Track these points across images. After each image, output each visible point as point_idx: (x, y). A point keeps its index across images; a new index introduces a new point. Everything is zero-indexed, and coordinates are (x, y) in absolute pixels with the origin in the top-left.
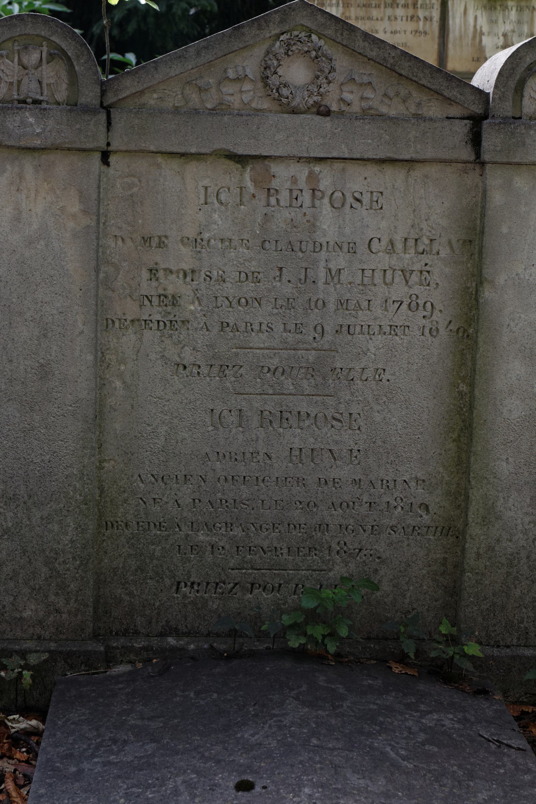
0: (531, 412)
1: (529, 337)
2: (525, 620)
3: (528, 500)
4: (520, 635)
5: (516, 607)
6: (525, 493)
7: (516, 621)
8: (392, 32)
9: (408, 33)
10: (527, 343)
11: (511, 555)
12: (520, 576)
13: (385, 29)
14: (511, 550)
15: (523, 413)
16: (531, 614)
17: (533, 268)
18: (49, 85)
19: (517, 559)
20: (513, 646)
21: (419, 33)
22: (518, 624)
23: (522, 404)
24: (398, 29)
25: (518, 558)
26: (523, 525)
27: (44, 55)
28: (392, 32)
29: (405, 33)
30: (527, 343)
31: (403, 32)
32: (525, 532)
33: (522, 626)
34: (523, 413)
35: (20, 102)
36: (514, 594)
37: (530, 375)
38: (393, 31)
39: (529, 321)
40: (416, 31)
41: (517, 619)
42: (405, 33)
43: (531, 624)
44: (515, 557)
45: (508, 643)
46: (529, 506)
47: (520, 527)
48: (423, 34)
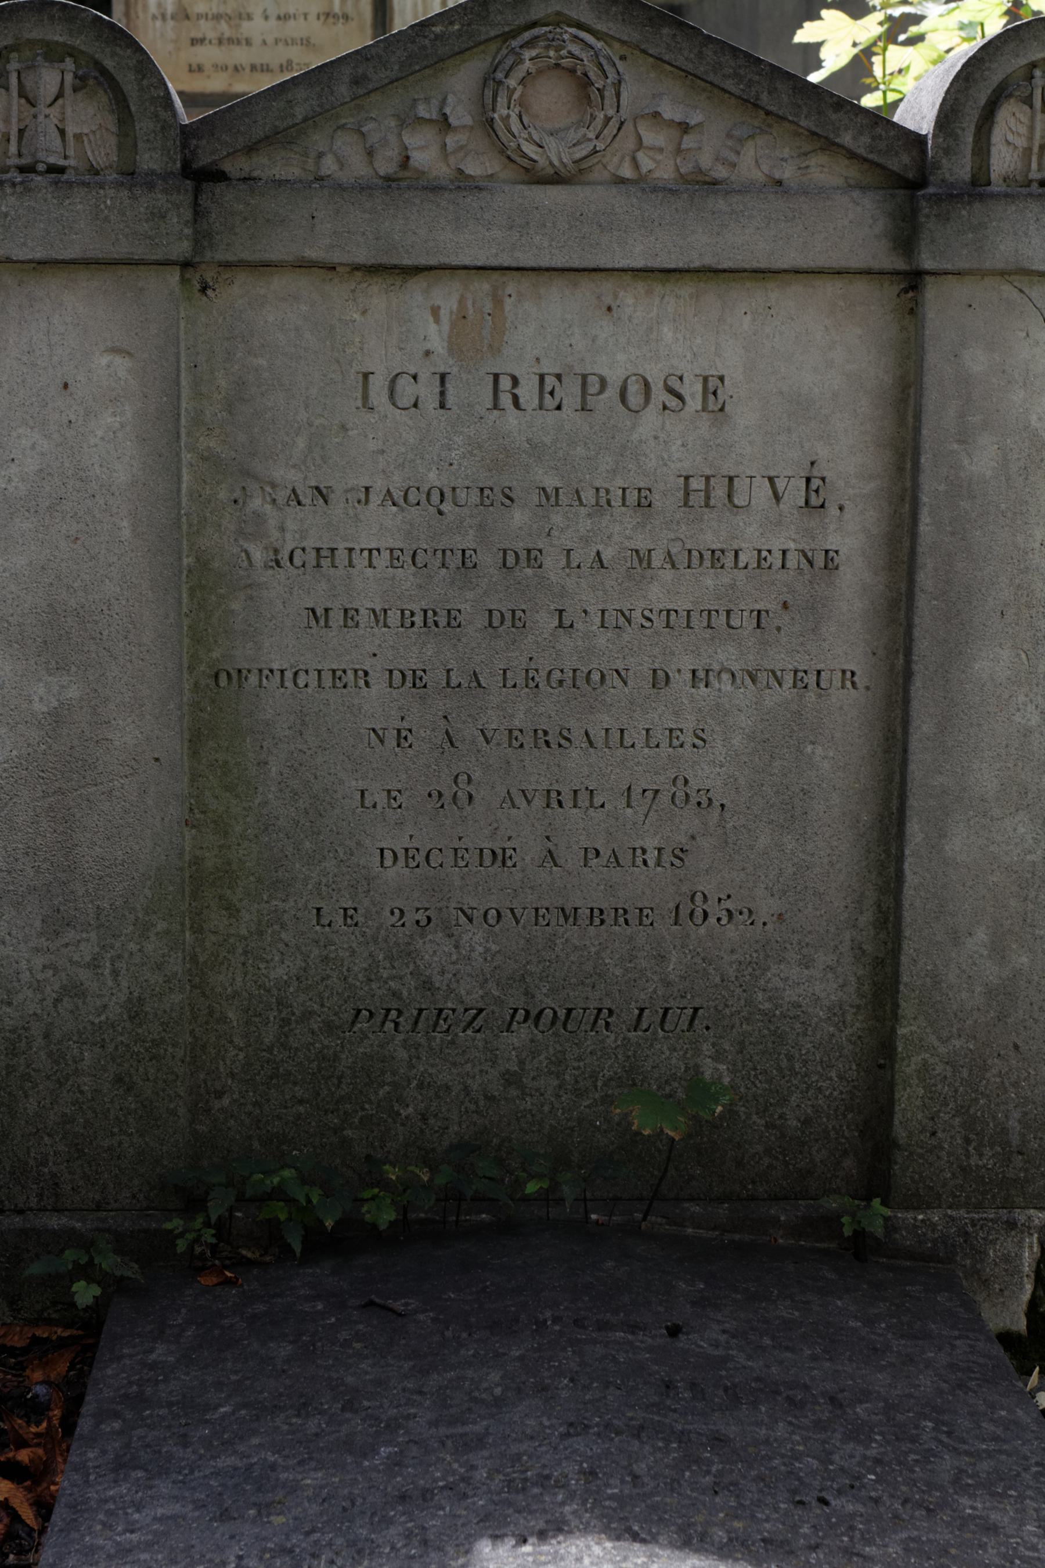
0: (30, 750)
1: (16, 603)
2: (51, 1159)
3: (38, 924)
4: (42, 1188)
5: (30, 1134)
6: (30, 909)
7: (32, 1162)
8: (279, 18)
9: (312, 17)
10: (12, 615)
11: (13, 1031)
12: (33, 1073)
13: (265, 10)
14: (11, 1022)
15: (15, 753)
16: (61, 1147)
17: (13, 465)
18: (78, 137)
19: (24, 1040)
20: (31, 1209)
21: (334, 17)
22: (37, 1167)
23: (11, 734)
24: (292, 11)
25: (26, 1037)
26: (31, 973)
27: (69, 78)
28: (279, 18)
29: (306, 19)
30: (12, 615)
31: (302, 17)
32: (38, 987)
33: (46, 1170)
34: (15, 753)
35: (22, 169)
36: (25, 1109)
37: (22, 676)
38: (282, 15)
39: (13, 571)
40: (328, 15)
41: (35, 1158)
42: (306, 19)
43: (62, 1167)
44: (19, 1035)
45: (21, 1205)
46: (41, 934)
47: (25, 977)
48: (341, 20)
